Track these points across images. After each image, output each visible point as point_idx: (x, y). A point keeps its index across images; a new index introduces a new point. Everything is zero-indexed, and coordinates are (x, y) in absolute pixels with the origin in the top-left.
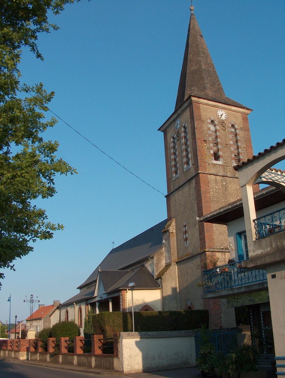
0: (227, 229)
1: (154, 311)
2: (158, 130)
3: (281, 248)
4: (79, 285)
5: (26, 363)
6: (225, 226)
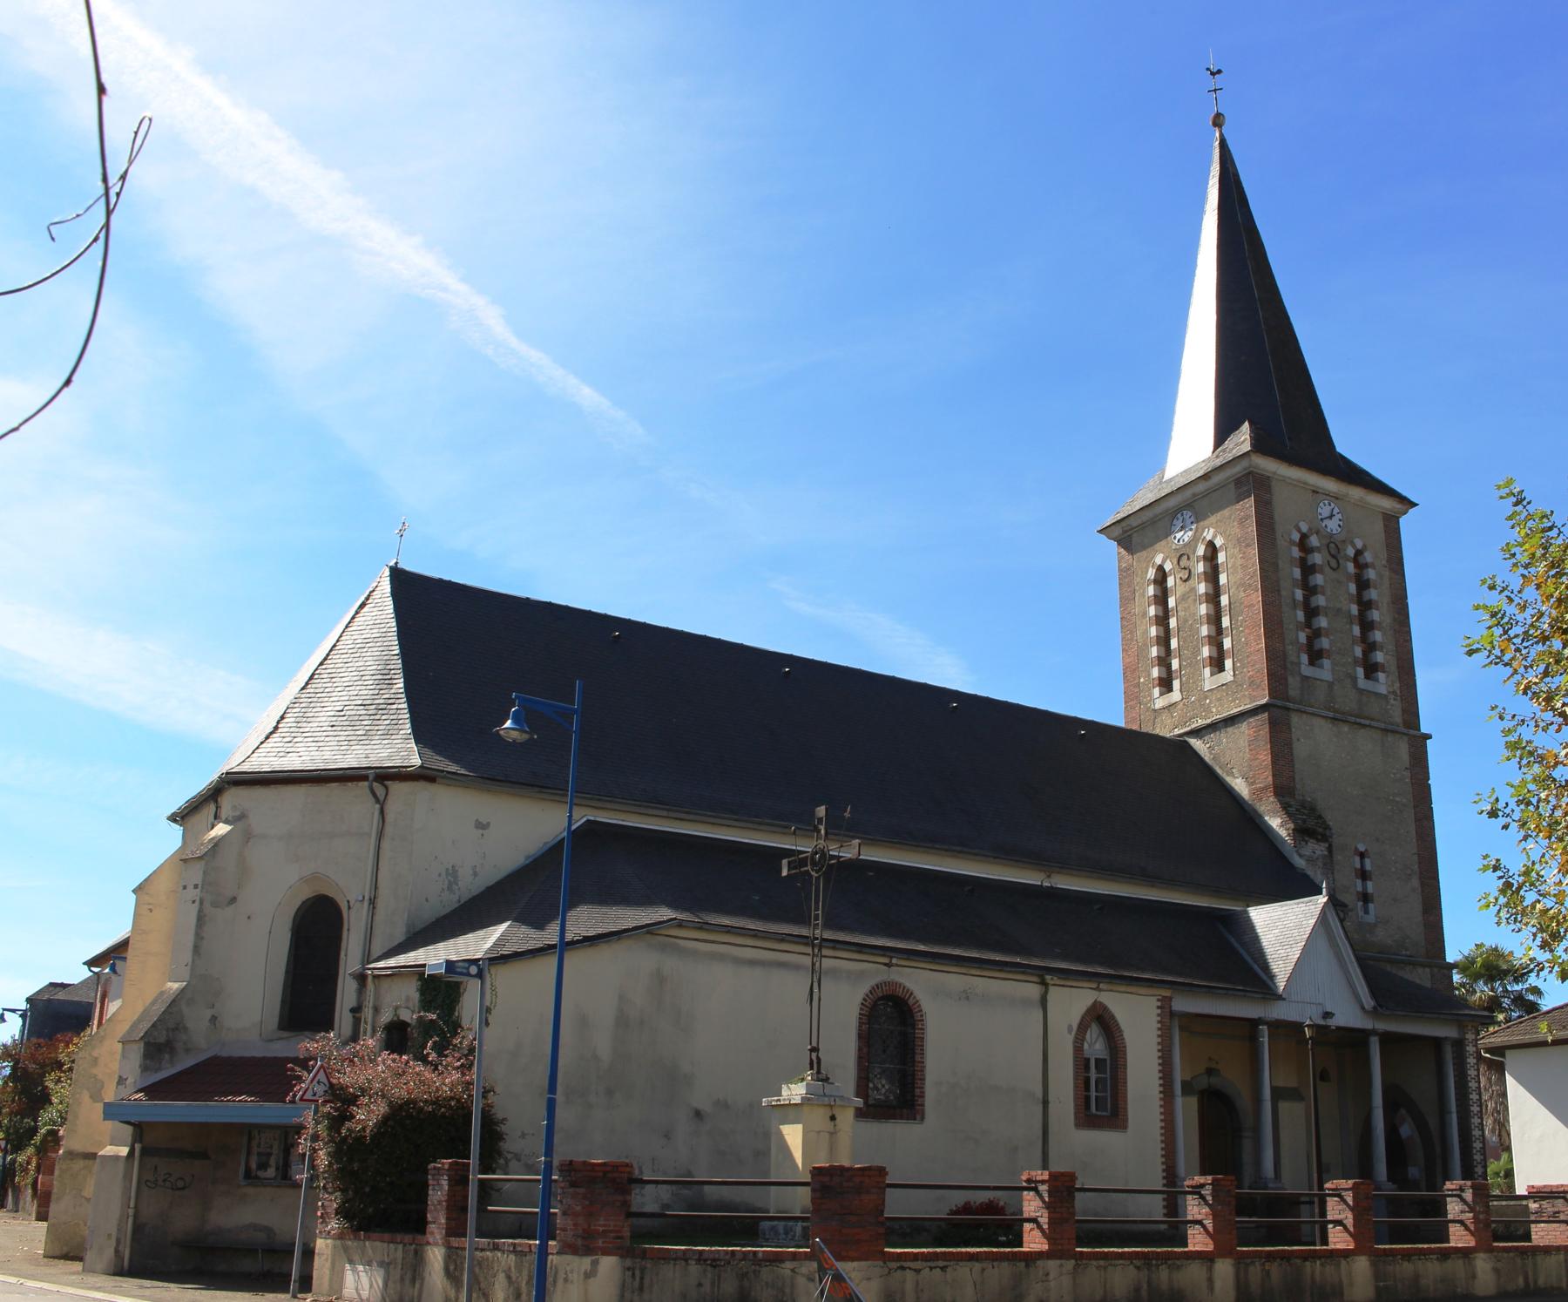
0: (1024, 1209)
1: (564, 838)
2: (1100, 531)
3: (1459, 1290)
4: (179, 798)
5: (1222, 467)
6: (1174, 682)
